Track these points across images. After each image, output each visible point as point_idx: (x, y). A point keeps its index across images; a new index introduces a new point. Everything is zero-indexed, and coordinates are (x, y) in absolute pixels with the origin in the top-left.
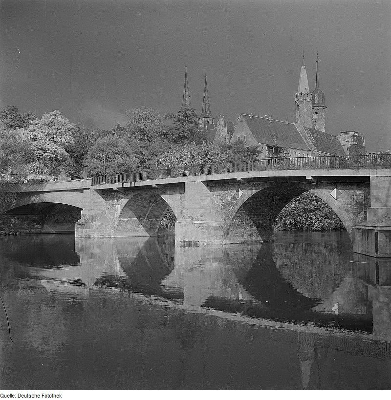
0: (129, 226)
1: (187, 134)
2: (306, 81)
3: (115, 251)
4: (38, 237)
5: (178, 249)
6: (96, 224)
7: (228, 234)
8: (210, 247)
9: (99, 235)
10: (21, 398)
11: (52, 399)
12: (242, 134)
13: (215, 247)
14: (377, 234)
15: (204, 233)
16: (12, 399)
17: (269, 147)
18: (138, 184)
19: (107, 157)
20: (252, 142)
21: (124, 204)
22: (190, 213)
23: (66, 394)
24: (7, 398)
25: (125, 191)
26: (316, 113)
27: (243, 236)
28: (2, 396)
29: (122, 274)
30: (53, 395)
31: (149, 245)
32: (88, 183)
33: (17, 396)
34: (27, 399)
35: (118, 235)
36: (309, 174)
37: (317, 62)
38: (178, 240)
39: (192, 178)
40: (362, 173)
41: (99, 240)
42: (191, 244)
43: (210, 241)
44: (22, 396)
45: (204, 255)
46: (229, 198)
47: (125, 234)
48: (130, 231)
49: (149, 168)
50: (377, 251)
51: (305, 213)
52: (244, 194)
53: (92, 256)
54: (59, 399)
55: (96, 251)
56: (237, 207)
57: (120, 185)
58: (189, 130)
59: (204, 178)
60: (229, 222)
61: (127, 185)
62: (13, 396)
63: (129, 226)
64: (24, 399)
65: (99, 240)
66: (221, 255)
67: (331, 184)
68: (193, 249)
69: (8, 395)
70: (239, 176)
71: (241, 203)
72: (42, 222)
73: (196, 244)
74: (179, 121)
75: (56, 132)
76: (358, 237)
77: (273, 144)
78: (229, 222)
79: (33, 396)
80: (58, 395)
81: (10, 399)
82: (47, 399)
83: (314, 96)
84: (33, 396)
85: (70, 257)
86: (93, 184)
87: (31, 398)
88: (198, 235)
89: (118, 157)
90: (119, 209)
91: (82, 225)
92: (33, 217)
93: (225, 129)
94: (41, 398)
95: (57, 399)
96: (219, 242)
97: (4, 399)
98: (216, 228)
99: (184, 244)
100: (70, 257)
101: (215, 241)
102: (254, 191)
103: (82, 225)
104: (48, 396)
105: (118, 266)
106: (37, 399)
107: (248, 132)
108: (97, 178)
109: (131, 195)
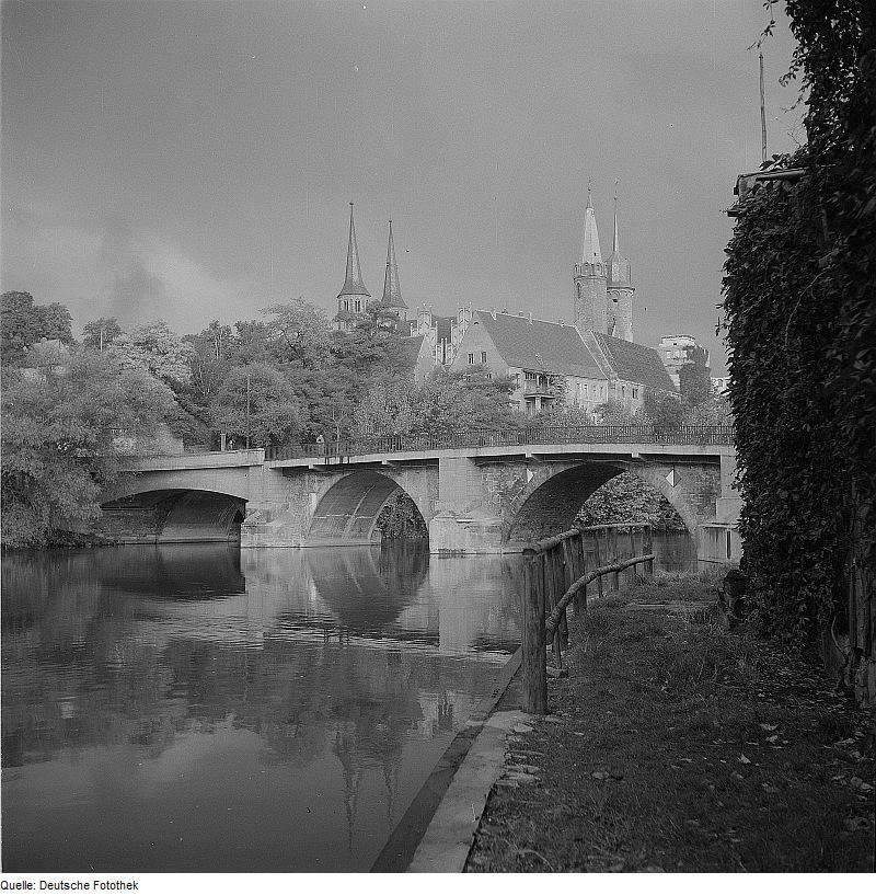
0: (328, 529)
1: (378, 352)
2: (595, 238)
3: (308, 571)
4: (152, 549)
5: (434, 561)
6: (276, 524)
7: (509, 538)
8: (483, 558)
9: (281, 544)
10: (47, 892)
11: (116, 892)
12: (477, 350)
13: (490, 558)
14: (729, 533)
15: (474, 537)
16: (27, 892)
17: (529, 374)
18: (355, 460)
19: (253, 405)
20: (499, 367)
21: (323, 492)
22: (451, 506)
23: (148, 881)
24: (16, 892)
25: (329, 470)
26: (615, 301)
27: (529, 541)
28: (4, 885)
29: (325, 610)
30: (119, 885)
32: (259, 455)
33: (37, 886)
34: (60, 892)
35: (311, 543)
36: (636, 451)
38: (434, 547)
39: (450, 453)
40: (709, 451)
41: (280, 551)
42: (454, 554)
43: (482, 549)
44: (50, 886)
45: (473, 570)
46: (510, 484)
47: (320, 542)
48: (328, 536)
49: (317, 421)
50: (729, 556)
51: (606, 499)
52: (533, 477)
53: (268, 579)
54: (132, 892)
55: (275, 570)
56: (524, 497)
57: (322, 462)
58: (380, 345)
59: (473, 453)
60: (511, 520)
61: (335, 461)
62: (29, 886)
63: (328, 529)
64: (54, 892)
65: (280, 551)
66: (498, 569)
67: (666, 464)
68: (456, 562)
69: (19, 885)
70: (529, 451)
71: (530, 491)
72: (160, 523)
73: (462, 554)
74: (361, 326)
75: (161, 359)
76: (704, 538)
77: (537, 370)
78: (511, 520)
79: (74, 886)
80: (129, 885)
81: (22, 892)
82: (106, 892)
83: (609, 268)
84: (74, 886)
85: (224, 579)
86: (269, 456)
87: (70, 892)
88: (466, 542)
89: (273, 404)
90: (314, 500)
91: (252, 527)
92: (142, 514)
93: (434, 333)
94: (91, 891)
95: (126, 892)
96: (495, 550)
97: (9, 892)
98: (491, 530)
99: (445, 554)
100: (224, 579)
101: (491, 550)
102: (551, 473)
103: (252, 527)
104: (107, 885)
105: (314, 594)
106: (84, 892)
107: (488, 345)
108: (274, 446)
109: (338, 477)
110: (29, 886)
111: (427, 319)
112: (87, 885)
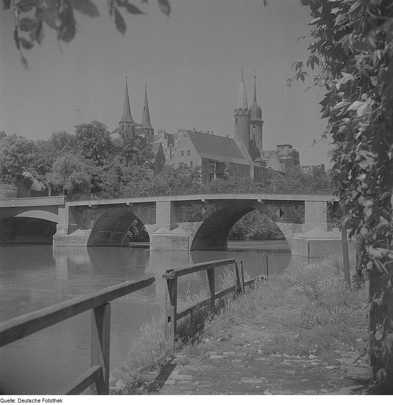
28: (2, 400)
30: (54, 401)
31: (367, 176)
33: (17, 401)
37: (255, 77)
44: (23, 401)
62: (13, 401)
69: (8, 400)
79: (33, 401)
80: (58, 400)
84: (33, 401)
110: (13, 401)
111: (163, 135)
112: (39, 400)
